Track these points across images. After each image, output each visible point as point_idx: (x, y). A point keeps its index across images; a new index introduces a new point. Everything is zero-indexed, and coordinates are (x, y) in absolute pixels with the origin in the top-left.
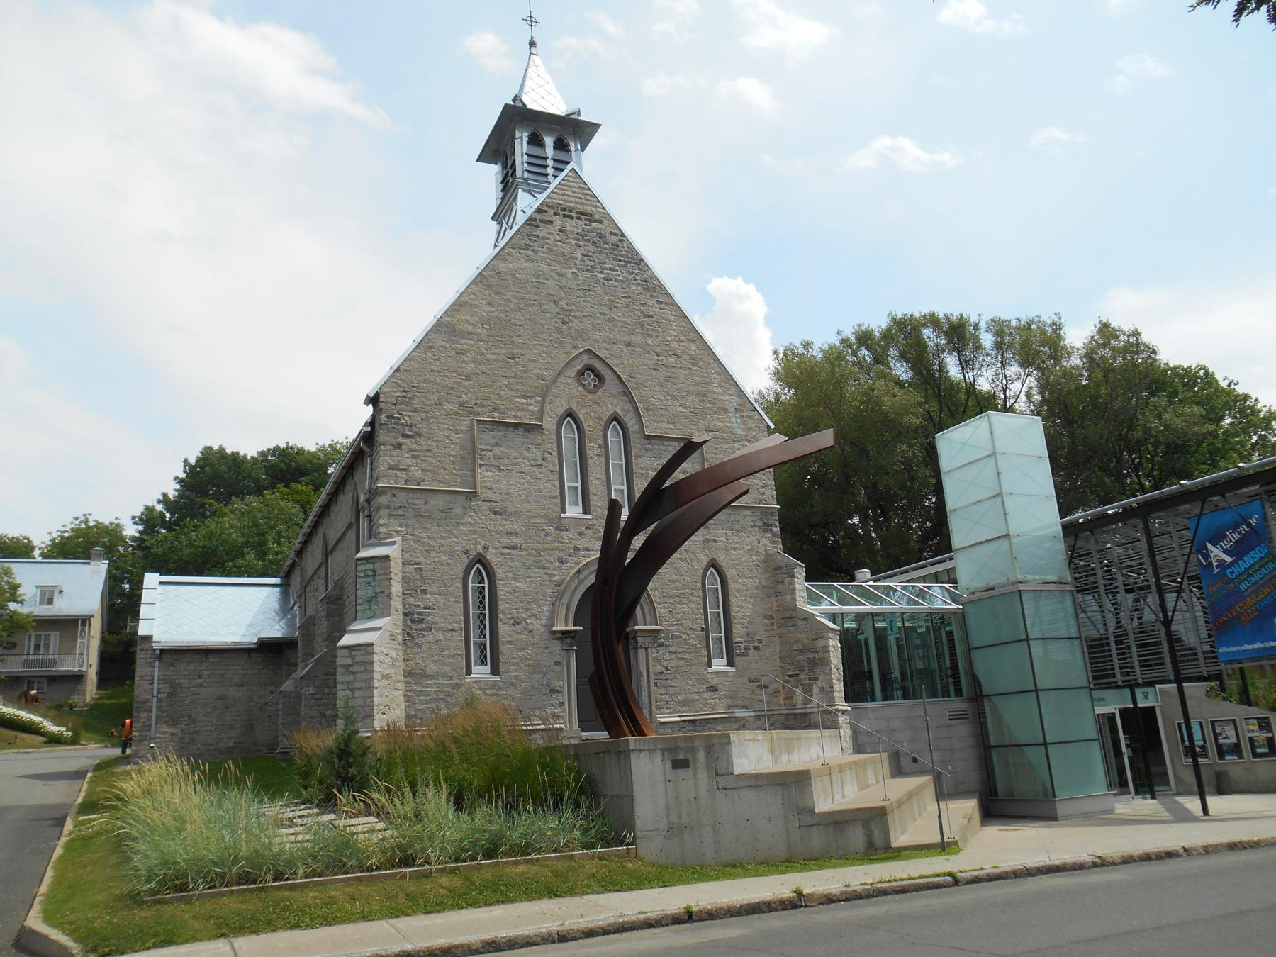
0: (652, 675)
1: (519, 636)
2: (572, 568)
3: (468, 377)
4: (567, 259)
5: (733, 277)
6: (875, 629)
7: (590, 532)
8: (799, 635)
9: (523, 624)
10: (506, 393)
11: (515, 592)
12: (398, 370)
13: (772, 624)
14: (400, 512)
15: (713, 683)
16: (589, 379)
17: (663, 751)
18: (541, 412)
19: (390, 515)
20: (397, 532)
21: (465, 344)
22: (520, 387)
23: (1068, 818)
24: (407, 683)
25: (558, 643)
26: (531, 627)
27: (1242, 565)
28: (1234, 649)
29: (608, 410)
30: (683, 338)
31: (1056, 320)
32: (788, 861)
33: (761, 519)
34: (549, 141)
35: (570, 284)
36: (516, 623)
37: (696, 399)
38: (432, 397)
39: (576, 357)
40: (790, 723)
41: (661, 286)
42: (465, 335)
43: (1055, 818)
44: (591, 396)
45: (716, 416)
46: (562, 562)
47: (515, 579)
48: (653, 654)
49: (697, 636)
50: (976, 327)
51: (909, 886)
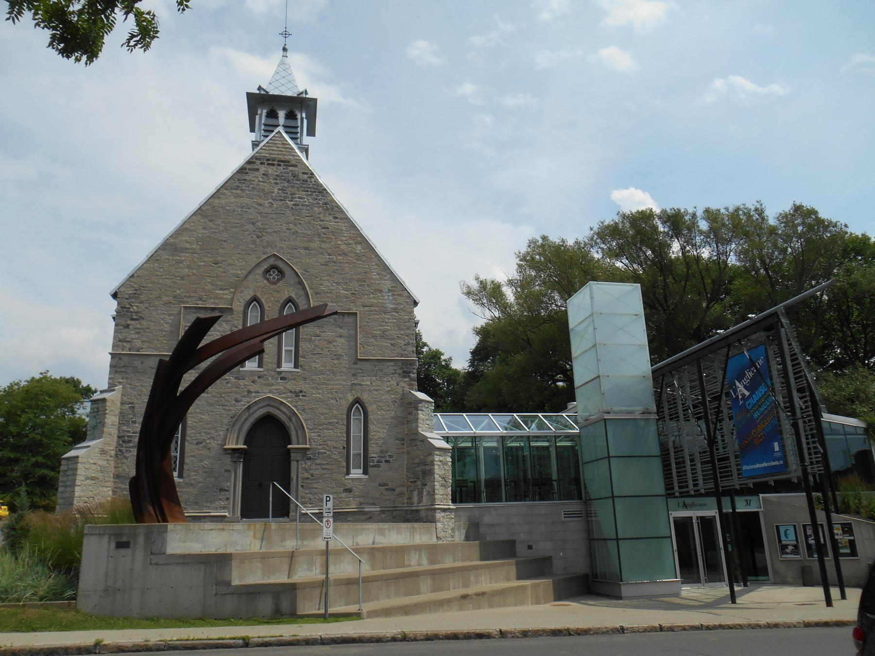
0: (300, 479)
1: (200, 452)
2: (244, 405)
3: (182, 278)
4: (266, 194)
5: (627, 188)
6: (556, 447)
7: (261, 380)
8: (418, 452)
9: (204, 444)
10: (210, 287)
11: (200, 422)
12: (132, 276)
13: (403, 444)
14: (124, 370)
15: (349, 486)
16: (274, 274)
17: (110, 536)
18: (232, 299)
19: (116, 372)
20: (120, 383)
21: (183, 256)
22: (219, 283)
23: (628, 598)
24: (115, 482)
25: (229, 456)
26: (209, 446)
27: (755, 398)
28: (751, 467)
29: (285, 296)
30: (351, 242)
31: (758, 206)
32: (201, 619)
33: (402, 368)
34: (282, 114)
35: (266, 210)
36: (198, 443)
37: (357, 284)
38: (154, 293)
39: (265, 260)
40: (409, 517)
41: (338, 206)
42: (184, 250)
43: (619, 598)
44: (273, 287)
45: (372, 296)
46: (237, 401)
47: (201, 413)
48: (302, 464)
49: (339, 453)
50: (694, 215)
51: (198, 645)
